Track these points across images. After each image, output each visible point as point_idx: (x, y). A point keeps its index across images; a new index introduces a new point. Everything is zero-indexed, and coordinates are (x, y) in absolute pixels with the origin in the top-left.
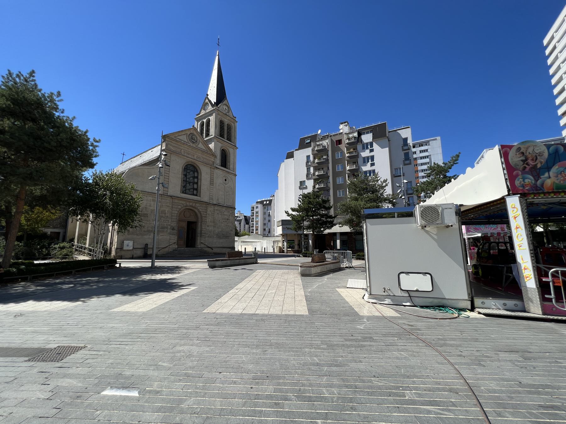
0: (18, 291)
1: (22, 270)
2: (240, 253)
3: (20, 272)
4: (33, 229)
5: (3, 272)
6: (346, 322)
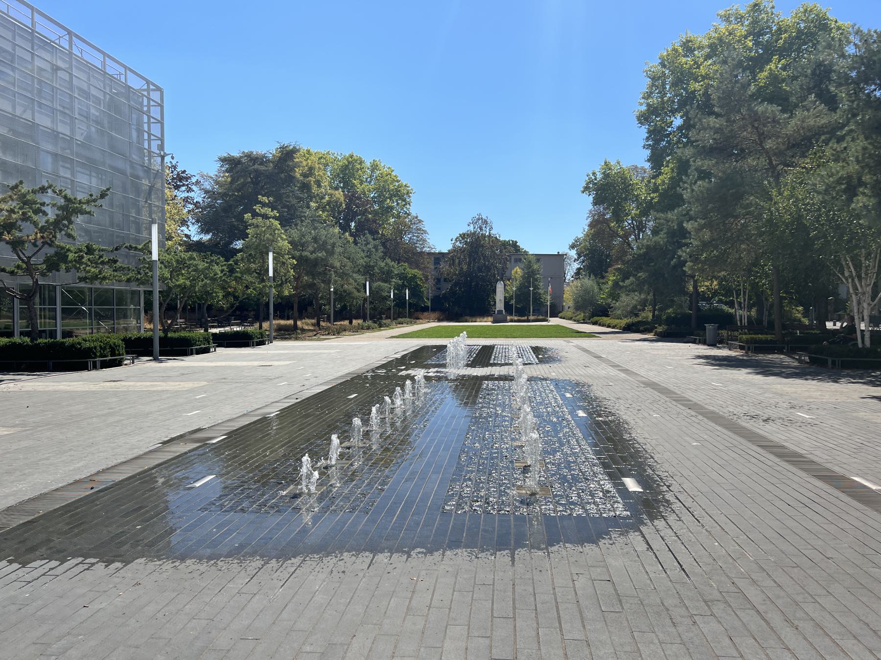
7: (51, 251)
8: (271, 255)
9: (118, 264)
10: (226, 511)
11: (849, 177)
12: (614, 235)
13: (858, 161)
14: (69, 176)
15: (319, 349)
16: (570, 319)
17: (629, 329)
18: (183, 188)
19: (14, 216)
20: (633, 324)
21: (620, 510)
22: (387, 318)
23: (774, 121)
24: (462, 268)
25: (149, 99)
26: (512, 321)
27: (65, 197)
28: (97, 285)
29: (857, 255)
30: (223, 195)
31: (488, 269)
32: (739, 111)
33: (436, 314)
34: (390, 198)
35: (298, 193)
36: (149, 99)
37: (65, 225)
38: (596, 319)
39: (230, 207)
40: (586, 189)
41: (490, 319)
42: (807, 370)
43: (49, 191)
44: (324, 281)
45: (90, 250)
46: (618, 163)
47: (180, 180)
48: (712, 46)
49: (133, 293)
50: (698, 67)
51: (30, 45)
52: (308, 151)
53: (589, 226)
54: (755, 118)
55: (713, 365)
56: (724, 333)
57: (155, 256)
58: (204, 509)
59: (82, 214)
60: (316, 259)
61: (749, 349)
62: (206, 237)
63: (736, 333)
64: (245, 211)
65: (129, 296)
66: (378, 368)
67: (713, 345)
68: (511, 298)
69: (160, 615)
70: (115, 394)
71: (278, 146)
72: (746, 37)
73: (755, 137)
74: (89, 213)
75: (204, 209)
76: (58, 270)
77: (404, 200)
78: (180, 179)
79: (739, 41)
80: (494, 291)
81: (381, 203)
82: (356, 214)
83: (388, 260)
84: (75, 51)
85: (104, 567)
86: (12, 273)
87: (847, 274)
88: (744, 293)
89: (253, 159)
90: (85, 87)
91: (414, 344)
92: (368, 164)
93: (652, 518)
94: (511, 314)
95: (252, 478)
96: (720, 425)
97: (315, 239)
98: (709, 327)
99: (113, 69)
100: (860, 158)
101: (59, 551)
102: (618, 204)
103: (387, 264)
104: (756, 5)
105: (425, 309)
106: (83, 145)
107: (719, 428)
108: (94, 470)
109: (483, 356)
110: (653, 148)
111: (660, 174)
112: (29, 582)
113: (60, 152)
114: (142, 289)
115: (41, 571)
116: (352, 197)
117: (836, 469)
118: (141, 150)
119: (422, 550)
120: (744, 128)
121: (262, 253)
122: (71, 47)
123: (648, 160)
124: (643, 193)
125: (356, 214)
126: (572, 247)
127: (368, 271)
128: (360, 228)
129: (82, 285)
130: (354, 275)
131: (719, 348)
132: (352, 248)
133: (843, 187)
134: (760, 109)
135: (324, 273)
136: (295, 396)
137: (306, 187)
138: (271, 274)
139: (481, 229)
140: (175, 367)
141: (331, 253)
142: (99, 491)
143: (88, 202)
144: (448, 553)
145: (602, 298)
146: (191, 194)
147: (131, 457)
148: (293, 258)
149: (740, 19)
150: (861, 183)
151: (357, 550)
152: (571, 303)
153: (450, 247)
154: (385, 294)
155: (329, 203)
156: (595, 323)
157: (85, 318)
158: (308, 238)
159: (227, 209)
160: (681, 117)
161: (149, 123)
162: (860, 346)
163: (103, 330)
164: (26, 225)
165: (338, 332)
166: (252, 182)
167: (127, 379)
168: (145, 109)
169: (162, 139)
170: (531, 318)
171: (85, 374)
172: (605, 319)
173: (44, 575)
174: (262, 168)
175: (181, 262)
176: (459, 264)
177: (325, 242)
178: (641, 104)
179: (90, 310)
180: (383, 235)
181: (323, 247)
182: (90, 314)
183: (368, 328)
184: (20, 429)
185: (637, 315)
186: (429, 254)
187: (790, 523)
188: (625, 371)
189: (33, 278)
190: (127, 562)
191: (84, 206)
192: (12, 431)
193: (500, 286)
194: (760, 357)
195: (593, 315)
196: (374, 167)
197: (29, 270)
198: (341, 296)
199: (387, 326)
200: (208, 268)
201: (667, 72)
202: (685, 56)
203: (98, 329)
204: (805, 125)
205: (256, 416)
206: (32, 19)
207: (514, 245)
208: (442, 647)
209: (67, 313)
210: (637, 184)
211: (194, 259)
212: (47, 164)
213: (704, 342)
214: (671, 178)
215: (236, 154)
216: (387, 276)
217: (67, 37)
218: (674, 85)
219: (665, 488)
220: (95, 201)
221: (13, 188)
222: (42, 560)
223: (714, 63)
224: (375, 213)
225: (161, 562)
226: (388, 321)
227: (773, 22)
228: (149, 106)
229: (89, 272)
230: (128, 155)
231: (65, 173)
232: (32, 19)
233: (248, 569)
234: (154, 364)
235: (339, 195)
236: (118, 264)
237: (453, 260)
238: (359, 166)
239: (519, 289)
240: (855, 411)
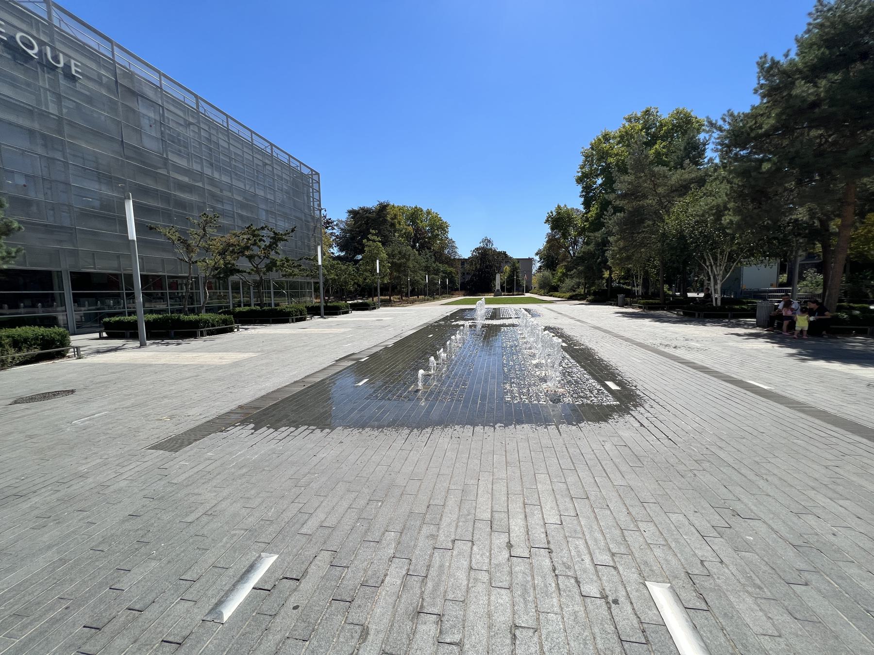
0: (857, 348)
1: (856, 316)
2: (788, 280)
3: (854, 319)
4: (861, 254)
5: (829, 317)
6: (811, 435)
7: (268, 261)
8: (378, 261)
9: (302, 267)
10: (379, 399)
11: (718, 206)
12: (561, 247)
13: (727, 195)
14: (274, 222)
15: (405, 311)
16: (536, 294)
17: (571, 298)
18: (330, 228)
19: (250, 242)
20: (573, 296)
21: (612, 401)
22: (436, 295)
23: (664, 177)
24: (476, 267)
25: (312, 179)
26: (504, 295)
27: (274, 232)
28: (291, 279)
29: (715, 252)
30: (350, 231)
31: (491, 267)
32: (643, 172)
33: (463, 292)
34: (437, 230)
35: (389, 228)
36: (312, 179)
37: (274, 247)
38: (551, 293)
39: (354, 237)
40: (547, 221)
41: (492, 294)
42: (684, 319)
43: (266, 229)
44: (405, 275)
45: (288, 261)
46: (565, 206)
47: (329, 223)
48: (622, 137)
49: (308, 283)
50: (612, 149)
51: (229, 178)
52: (393, 206)
53: (547, 242)
54: (653, 174)
55: (626, 317)
56: (628, 299)
57: (320, 263)
58: (367, 398)
59: (283, 241)
60: (401, 263)
61: (645, 308)
62: (343, 254)
63: (635, 300)
64: (362, 238)
65: (306, 285)
66: (440, 321)
67: (622, 306)
68: (504, 283)
69: (358, 462)
70: (306, 335)
71: (378, 203)
72: (641, 130)
73: (651, 186)
74: (286, 240)
75: (340, 238)
76: (272, 271)
77: (445, 231)
78: (328, 223)
79: (637, 133)
80: (495, 279)
81: (432, 233)
82: (419, 239)
83: (437, 263)
84: (274, 154)
85: (320, 432)
86: (249, 273)
87: (708, 264)
88: (640, 277)
89: (366, 211)
90: (280, 174)
91: (455, 308)
92: (425, 210)
93: (635, 406)
94: (504, 291)
95: (389, 380)
96: (649, 350)
97: (400, 253)
98: (620, 296)
99: (294, 164)
100: (728, 192)
101: (294, 422)
102: (565, 229)
103: (437, 265)
104: (647, 111)
105: (457, 290)
106: (280, 205)
107: (649, 352)
108: (303, 377)
109: (495, 315)
110: (585, 196)
111: (590, 211)
112: (281, 440)
113: (269, 209)
114: (312, 281)
115: (286, 434)
116: (417, 230)
117: (733, 375)
118: (309, 207)
119: (501, 425)
120: (645, 181)
121: (372, 261)
122: (272, 152)
123: (582, 204)
124: (579, 223)
125: (419, 239)
126: (537, 254)
127: (427, 269)
128: (422, 247)
129: (284, 279)
130: (420, 272)
131: (627, 308)
132: (419, 258)
133: (714, 211)
134: (656, 169)
135: (405, 271)
136: (400, 336)
137: (393, 225)
138: (378, 272)
139: (487, 245)
140: (332, 321)
141: (408, 260)
142: (309, 387)
143: (285, 235)
144: (518, 426)
145: (554, 282)
146: (334, 231)
147: (321, 369)
148: (389, 263)
149: (637, 120)
150: (726, 208)
151: (463, 423)
152: (537, 285)
153: (470, 255)
154: (436, 281)
155: (405, 233)
156: (551, 296)
157: (285, 297)
158: (396, 252)
159: (353, 238)
160: (602, 179)
161: (313, 192)
162: (714, 305)
163: (293, 303)
164: (255, 248)
165: (413, 302)
166: (365, 223)
167: (309, 327)
168: (311, 185)
169: (320, 201)
170: (515, 293)
171: (288, 325)
172: (556, 293)
173: (288, 435)
174: (370, 215)
175: (332, 266)
176: (475, 264)
177: (405, 254)
178: (578, 172)
179: (287, 292)
180: (433, 250)
181: (404, 256)
182: (288, 294)
183: (428, 300)
184: (260, 353)
185: (574, 291)
186: (459, 259)
187: (725, 410)
188: (579, 321)
189: (260, 275)
190: (332, 429)
191: (284, 237)
192: (257, 354)
193: (498, 277)
194: (652, 312)
195: (549, 291)
196: (429, 213)
197: (258, 271)
198: (413, 283)
199: (438, 299)
200: (346, 269)
201: (594, 152)
202: (605, 143)
203: (291, 303)
204: (682, 178)
205: (382, 346)
206: (252, 137)
207: (505, 253)
208: (537, 488)
209: (276, 294)
210: (576, 218)
211: (339, 264)
212: (263, 216)
213: (617, 305)
214: (596, 214)
215: (356, 208)
216: (437, 272)
217: (270, 147)
218: (599, 160)
219: (634, 388)
220: (289, 234)
221: (248, 228)
222: (285, 427)
223: (623, 146)
224: (429, 238)
225: (351, 429)
226: (437, 296)
227: (657, 120)
228: (312, 183)
229: (287, 272)
230: (303, 209)
231: (272, 220)
232: (252, 137)
233: (402, 435)
234: (322, 320)
235: (410, 229)
236: (302, 267)
237: (472, 263)
238: (420, 213)
239: (508, 277)
240: (725, 342)
